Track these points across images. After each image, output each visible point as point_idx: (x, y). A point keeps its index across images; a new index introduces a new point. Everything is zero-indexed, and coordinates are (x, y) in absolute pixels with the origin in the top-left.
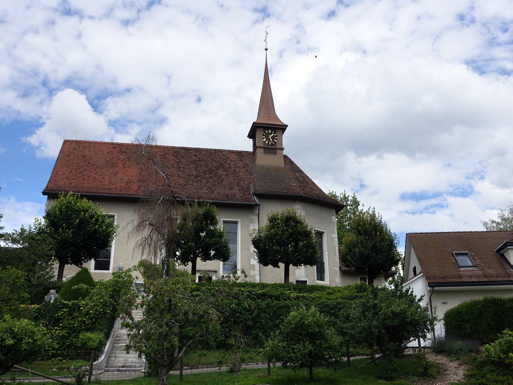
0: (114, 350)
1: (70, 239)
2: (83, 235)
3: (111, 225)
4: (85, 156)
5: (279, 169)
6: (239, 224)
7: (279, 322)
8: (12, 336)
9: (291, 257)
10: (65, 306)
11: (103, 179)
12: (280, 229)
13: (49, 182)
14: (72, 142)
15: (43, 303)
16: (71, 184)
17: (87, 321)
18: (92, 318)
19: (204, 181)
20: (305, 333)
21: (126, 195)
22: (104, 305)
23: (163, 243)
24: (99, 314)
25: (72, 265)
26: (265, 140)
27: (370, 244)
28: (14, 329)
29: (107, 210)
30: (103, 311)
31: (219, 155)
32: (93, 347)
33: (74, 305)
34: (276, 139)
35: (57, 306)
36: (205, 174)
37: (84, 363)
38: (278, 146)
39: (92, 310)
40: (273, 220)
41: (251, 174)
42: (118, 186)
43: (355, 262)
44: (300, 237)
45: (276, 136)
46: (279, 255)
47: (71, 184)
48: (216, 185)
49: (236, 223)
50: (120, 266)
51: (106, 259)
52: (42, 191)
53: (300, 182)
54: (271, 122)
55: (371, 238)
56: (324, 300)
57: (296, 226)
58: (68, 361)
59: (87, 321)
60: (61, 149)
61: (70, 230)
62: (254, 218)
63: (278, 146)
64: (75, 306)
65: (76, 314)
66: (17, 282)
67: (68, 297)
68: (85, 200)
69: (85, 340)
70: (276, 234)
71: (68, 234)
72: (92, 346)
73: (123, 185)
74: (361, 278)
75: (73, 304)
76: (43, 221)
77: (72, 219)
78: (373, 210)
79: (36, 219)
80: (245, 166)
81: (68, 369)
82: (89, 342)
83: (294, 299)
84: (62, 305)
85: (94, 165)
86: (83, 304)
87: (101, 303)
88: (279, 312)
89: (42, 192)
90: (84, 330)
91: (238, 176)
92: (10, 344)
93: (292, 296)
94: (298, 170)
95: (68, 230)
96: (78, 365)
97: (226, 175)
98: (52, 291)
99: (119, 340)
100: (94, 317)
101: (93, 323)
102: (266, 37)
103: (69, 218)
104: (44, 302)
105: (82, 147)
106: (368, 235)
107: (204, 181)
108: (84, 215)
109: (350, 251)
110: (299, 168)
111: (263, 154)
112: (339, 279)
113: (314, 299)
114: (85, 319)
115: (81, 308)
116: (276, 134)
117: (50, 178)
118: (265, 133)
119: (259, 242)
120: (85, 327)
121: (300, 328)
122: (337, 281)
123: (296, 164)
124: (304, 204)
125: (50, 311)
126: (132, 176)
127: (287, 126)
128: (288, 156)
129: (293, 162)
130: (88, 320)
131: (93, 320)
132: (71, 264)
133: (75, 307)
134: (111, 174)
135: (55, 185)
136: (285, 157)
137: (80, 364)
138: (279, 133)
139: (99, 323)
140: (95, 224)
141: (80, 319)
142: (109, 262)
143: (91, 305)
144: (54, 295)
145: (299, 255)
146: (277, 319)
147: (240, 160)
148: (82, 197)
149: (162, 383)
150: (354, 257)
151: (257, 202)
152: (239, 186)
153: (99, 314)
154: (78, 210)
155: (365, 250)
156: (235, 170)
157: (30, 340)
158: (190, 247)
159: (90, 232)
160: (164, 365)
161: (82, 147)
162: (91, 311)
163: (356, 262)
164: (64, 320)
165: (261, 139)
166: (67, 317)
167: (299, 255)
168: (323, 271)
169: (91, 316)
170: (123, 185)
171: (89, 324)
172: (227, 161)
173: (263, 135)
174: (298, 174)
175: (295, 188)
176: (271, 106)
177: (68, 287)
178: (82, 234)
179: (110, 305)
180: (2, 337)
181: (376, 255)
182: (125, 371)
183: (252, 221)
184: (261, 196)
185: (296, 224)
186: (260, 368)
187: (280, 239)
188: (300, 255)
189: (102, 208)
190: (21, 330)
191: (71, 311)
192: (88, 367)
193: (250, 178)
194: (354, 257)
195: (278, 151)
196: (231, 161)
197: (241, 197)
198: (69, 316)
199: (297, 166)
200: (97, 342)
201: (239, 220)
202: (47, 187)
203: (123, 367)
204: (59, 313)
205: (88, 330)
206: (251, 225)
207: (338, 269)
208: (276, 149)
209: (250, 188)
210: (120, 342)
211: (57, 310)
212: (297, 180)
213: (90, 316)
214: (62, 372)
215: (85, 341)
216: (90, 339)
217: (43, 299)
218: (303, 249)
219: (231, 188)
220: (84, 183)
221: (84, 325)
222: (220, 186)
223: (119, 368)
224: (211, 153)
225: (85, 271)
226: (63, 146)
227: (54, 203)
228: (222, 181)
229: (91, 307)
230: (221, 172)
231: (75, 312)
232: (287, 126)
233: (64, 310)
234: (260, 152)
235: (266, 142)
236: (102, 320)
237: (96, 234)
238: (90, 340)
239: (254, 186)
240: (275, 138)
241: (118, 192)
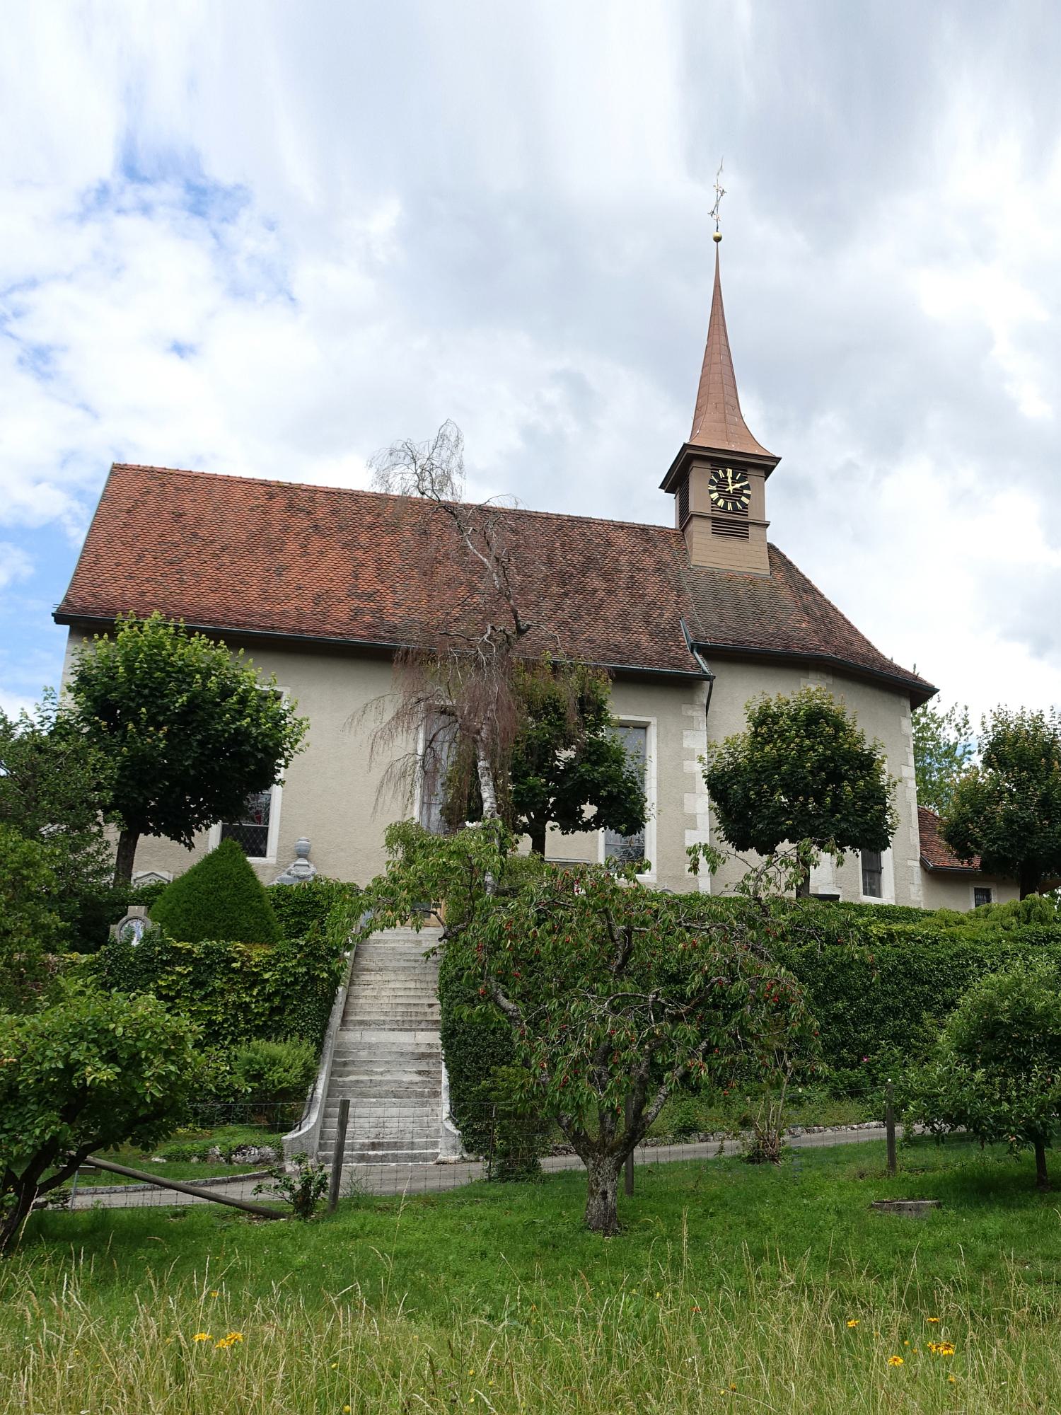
0: (334, 1096)
1: (159, 755)
2: (202, 744)
3: (277, 720)
4: (181, 515)
5: (755, 581)
6: (652, 732)
7: (844, 1008)
8: (104, 1053)
9: (821, 824)
10: (180, 957)
11: (241, 583)
12: (792, 745)
13: (73, 585)
14: (138, 471)
15: (103, 948)
16: (143, 594)
17: (253, 1006)
18: (270, 995)
19: (546, 604)
20: (1035, 1039)
21: (319, 632)
22: (311, 954)
23: (487, 769)
24: (296, 982)
25: (159, 836)
26: (715, 496)
27: (1036, 792)
28: (112, 1026)
29: (273, 673)
30: (307, 973)
31: (584, 534)
32: (284, 1085)
33: (212, 953)
34: (748, 496)
35: (153, 959)
36: (548, 586)
37: (255, 1137)
38: (752, 516)
39: (270, 970)
40: (764, 720)
41: (680, 592)
42: (290, 606)
43: (994, 841)
44: (846, 770)
45: (747, 487)
46: (788, 819)
47: (143, 594)
48: (581, 617)
49: (644, 727)
50: (301, 845)
51: (255, 822)
52: (54, 611)
53: (815, 620)
54: (733, 447)
55: (1036, 777)
56: (967, 945)
57: (836, 738)
58: (194, 1131)
59: (253, 1006)
60: (106, 490)
61: (158, 728)
62: (695, 714)
63: (752, 516)
64: (215, 957)
65: (218, 984)
66: (27, 878)
67: (181, 929)
68: (198, 641)
69: (259, 1063)
70: (779, 761)
71: (154, 741)
72: (280, 1083)
73: (307, 606)
74: (975, 889)
75: (209, 952)
76: (69, 701)
77: (166, 696)
78: (965, 712)
79: (46, 690)
80: (661, 567)
81: (204, 1157)
82: (270, 1070)
83: (881, 939)
84: (168, 952)
85: (212, 542)
86: (239, 952)
87: (301, 948)
88: (842, 978)
89: (53, 614)
90: (246, 1032)
91: (642, 596)
92: (101, 1081)
93: (875, 932)
94: (804, 587)
95: (151, 729)
96: (233, 1143)
97: (609, 592)
98: (134, 910)
99: (345, 1064)
100: (276, 993)
101: (274, 1011)
102: (718, 201)
103: (158, 691)
104: (106, 944)
105: (169, 489)
106: (1026, 769)
107: (546, 604)
108: (204, 685)
109: (978, 813)
110: (808, 582)
111: (710, 536)
112: (921, 893)
113: (936, 942)
114: (248, 999)
115: (234, 965)
116: (746, 483)
117: (76, 574)
118: (717, 476)
119: (728, 781)
120: (247, 1022)
121: (1021, 1023)
122: (913, 898)
123: (801, 570)
124: (830, 680)
125: (131, 972)
126: (332, 580)
127: (780, 459)
128: (777, 546)
129: (791, 563)
130: (257, 1001)
131: (277, 1002)
132: (157, 834)
133: (213, 962)
134: (267, 571)
135: (93, 595)
136: (771, 548)
137: (239, 1141)
138: (753, 478)
139: (292, 1011)
140: (240, 714)
141: (232, 998)
142: (265, 832)
143: (267, 956)
144: (143, 921)
145: (844, 819)
146: (837, 999)
147: (645, 550)
148: (190, 632)
149: (602, 1203)
150: (988, 828)
151: (705, 668)
152: (648, 623)
153: (296, 982)
154: (180, 670)
155: (1021, 809)
156: (632, 577)
157: (173, 1068)
158: (531, 788)
159: (223, 736)
160: (605, 1146)
161: (169, 489)
162: (267, 972)
163: (994, 843)
164: (177, 1001)
165: (702, 493)
166: (186, 992)
167: (844, 819)
168: (879, 871)
169: (269, 989)
170: (307, 606)
171: (262, 1015)
172: (606, 552)
173: (712, 483)
174: (808, 598)
175: (801, 633)
176: (732, 401)
177: (178, 901)
178: (197, 740)
179: (327, 955)
180: (68, 1055)
181: (1050, 826)
182: (383, 1159)
183: (689, 723)
184: (714, 654)
185: (837, 732)
186: (831, 1143)
187: (792, 773)
188: (848, 821)
189: (255, 666)
190: (137, 1031)
191: (199, 972)
192: (268, 1149)
193: (677, 603)
194: (988, 828)
195: (752, 530)
196: (621, 552)
197: (657, 653)
198: (195, 988)
199: (803, 576)
200: (298, 1070)
201: (653, 720)
202: (66, 600)
203: (374, 1146)
204: (160, 978)
205: (261, 1032)
206: (687, 736)
207: (918, 864)
208: (747, 524)
209: (680, 631)
210: (349, 1068)
211: (154, 971)
212: (808, 614)
213: (264, 988)
214: (183, 1166)
215: (257, 1067)
216: (274, 1062)
217: (103, 938)
218: (855, 803)
219: (626, 629)
220: (184, 595)
221: (245, 1016)
222: (595, 620)
223: (361, 1149)
224: (560, 528)
225: (231, 851)
226: (109, 481)
227: (97, 650)
228: (599, 607)
229: (268, 963)
230: (593, 581)
231: (216, 978)
232: (780, 459)
233: (178, 969)
234: (700, 532)
235: (719, 504)
236: (302, 1000)
237: (241, 743)
238: (274, 1064)
239: (692, 624)
240: (745, 492)
241: (292, 624)
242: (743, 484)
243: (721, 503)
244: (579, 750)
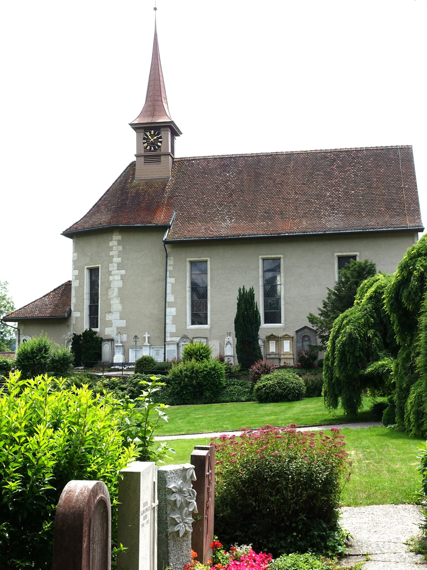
26: (146, 144)
34: (161, 142)
195: (163, 158)
240: (160, 140)
242: (159, 136)
243: (148, 148)
244: (328, 551)
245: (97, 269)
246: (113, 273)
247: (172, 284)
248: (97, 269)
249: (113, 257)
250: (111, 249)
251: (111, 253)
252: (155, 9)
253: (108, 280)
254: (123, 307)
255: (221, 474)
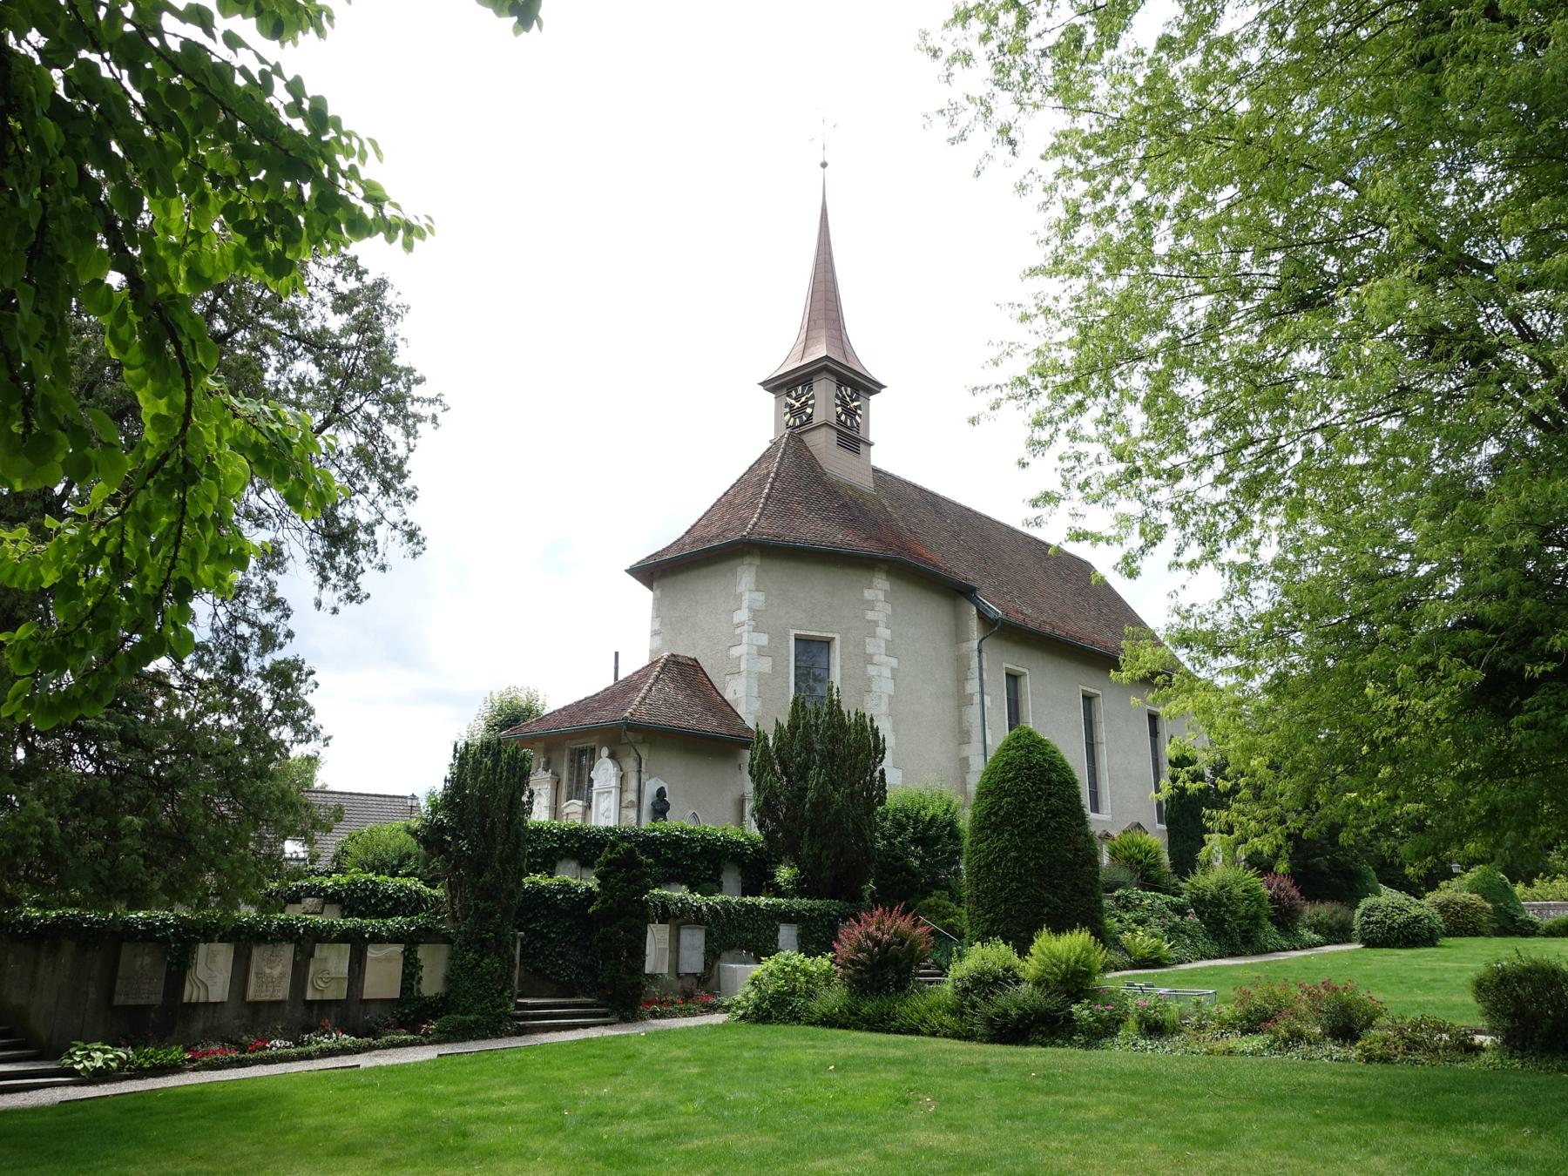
245: (827, 643)
246: (876, 659)
247: (889, 696)
248: (827, 643)
249: (876, 623)
250: (871, 605)
251: (870, 615)
252: (824, 165)
253: (864, 673)
254: (897, 738)
255: (1309, 1043)
